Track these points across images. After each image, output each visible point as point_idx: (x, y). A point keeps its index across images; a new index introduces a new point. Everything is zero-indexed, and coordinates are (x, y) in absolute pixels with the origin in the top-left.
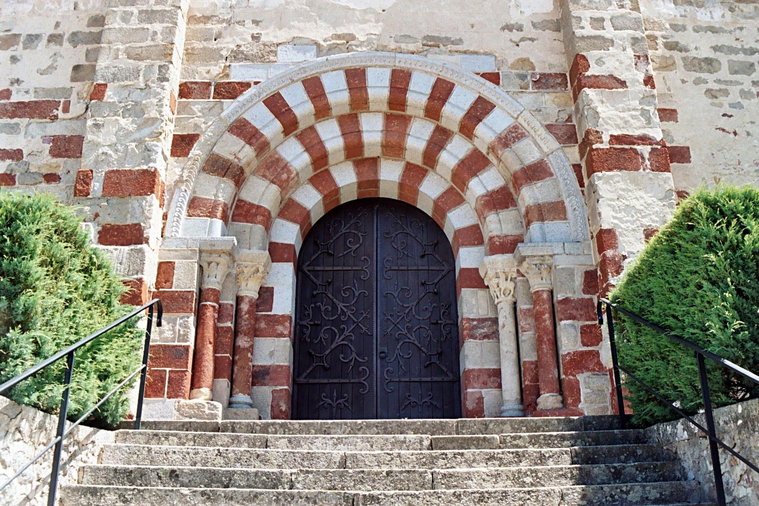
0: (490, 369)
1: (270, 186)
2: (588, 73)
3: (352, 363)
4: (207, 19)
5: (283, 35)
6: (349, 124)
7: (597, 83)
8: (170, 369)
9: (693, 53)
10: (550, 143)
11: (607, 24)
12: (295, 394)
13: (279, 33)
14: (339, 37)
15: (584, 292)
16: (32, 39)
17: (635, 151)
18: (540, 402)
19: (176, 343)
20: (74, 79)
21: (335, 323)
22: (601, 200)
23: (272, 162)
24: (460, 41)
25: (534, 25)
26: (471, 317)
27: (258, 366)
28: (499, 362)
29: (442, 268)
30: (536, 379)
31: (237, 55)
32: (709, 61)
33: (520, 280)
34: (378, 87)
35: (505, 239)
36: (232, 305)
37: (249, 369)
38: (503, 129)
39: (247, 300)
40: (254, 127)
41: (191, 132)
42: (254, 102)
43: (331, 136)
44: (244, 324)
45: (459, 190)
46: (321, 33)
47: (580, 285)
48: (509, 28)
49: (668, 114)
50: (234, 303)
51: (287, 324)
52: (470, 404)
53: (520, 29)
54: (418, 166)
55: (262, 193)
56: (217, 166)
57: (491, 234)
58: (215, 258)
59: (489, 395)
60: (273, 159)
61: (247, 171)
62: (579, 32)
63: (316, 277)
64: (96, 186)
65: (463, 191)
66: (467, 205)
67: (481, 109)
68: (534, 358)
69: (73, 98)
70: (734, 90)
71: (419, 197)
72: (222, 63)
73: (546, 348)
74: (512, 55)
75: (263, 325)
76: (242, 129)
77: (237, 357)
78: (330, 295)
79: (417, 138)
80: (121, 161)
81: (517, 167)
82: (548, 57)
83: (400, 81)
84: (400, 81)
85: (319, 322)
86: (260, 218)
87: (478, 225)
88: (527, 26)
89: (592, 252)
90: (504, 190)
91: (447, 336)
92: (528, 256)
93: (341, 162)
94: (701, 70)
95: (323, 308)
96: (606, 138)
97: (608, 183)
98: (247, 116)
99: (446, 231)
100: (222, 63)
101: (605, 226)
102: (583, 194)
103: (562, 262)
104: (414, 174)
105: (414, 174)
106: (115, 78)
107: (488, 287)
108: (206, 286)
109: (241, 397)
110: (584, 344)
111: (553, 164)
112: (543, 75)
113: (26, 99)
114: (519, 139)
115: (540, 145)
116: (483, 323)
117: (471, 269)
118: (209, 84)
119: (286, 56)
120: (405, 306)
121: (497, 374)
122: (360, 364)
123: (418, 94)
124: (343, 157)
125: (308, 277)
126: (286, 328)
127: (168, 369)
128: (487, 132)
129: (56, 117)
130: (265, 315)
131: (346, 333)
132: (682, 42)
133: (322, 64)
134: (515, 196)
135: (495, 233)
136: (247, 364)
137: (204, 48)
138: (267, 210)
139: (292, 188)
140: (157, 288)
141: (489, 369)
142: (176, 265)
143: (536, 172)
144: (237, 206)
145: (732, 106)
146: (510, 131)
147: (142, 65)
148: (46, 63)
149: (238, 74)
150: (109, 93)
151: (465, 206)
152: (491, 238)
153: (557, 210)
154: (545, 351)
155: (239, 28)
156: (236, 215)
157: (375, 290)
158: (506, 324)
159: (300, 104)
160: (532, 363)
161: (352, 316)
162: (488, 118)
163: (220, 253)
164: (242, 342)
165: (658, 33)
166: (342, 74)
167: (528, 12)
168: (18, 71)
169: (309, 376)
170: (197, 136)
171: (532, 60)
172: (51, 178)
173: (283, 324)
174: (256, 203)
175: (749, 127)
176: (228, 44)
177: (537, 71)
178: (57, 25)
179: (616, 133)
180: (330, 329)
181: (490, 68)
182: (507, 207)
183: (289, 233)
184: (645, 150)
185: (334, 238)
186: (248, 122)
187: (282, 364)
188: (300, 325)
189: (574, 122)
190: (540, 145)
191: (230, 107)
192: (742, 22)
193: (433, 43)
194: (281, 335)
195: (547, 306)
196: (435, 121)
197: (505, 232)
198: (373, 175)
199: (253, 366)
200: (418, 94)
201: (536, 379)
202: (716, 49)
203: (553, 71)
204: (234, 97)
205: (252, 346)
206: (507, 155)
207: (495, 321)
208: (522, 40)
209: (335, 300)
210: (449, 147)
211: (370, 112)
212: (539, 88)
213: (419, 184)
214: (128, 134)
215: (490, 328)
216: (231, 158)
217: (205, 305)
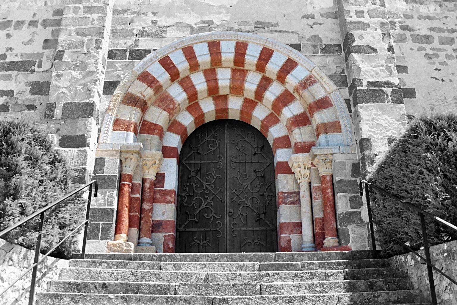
0: (295, 223)
2: (354, 44)
3: (212, 219)
4: (124, 11)
5: (170, 21)
6: (210, 75)
7: (360, 50)
8: (103, 222)
9: (418, 32)
10: (331, 86)
11: (366, 14)
13: (168, 20)
14: (204, 22)
16: (19, 24)
17: (382, 91)
19: (106, 207)
20: (44, 48)
22: (362, 121)
23: (164, 98)
24: (277, 25)
25: (322, 15)
26: (284, 191)
27: (155, 221)
28: (300, 218)
29: (266, 161)
30: (323, 228)
31: (143, 33)
32: (427, 37)
33: (313, 169)
34: (228, 53)
36: (140, 184)
37: (150, 222)
38: (303, 78)
39: (148, 181)
40: (153, 77)
42: (153, 62)
43: (199, 82)
44: (147, 195)
45: (276, 115)
46: (194, 20)
48: (306, 17)
49: (402, 69)
50: (141, 183)
52: (283, 244)
53: (313, 17)
55: (158, 116)
56: (131, 100)
57: (295, 141)
58: (129, 155)
59: (294, 238)
60: (165, 96)
61: (149, 103)
62: (348, 19)
63: (191, 167)
64: (58, 112)
65: (279, 115)
67: (289, 66)
68: (321, 216)
69: (44, 59)
70: (442, 54)
72: (134, 38)
74: (308, 33)
75: (158, 196)
76: (146, 78)
77: (143, 215)
79: (251, 83)
80: (73, 97)
81: (311, 101)
82: (329, 34)
83: (241, 49)
84: (241, 49)
86: (156, 131)
87: (288, 135)
88: (318, 16)
91: (269, 202)
92: (318, 155)
94: (422, 42)
95: (194, 186)
96: (365, 83)
97: (367, 111)
98: (149, 70)
99: (268, 139)
100: (134, 38)
101: (364, 136)
102: (351, 117)
103: (339, 158)
104: (249, 105)
105: (249, 105)
106: (69, 47)
107: (294, 173)
108: (124, 173)
109: (145, 240)
110: (352, 208)
111: (333, 99)
112: (327, 46)
113: (16, 60)
114: (312, 84)
115: (325, 88)
116: (291, 195)
118: (126, 51)
119: (173, 34)
121: (299, 225)
123: (252, 57)
124: (206, 95)
125: (186, 167)
126: (172, 198)
127: (101, 223)
128: (293, 79)
129: (34, 71)
130: (160, 190)
131: (208, 201)
132: (411, 26)
133: (194, 39)
135: (298, 141)
136: (149, 220)
137: (123, 29)
138: (161, 126)
139: (176, 113)
140: (95, 174)
143: (323, 104)
144: (143, 124)
145: (441, 64)
146: (307, 79)
147: (86, 39)
148: (28, 38)
149: (144, 44)
150: (65, 56)
152: (296, 144)
154: (328, 211)
155: (144, 17)
156: (142, 130)
158: (305, 195)
159: (181, 63)
160: (320, 219)
161: (212, 191)
162: (294, 71)
163: (132, 153)
164: (146, 206)
165: (396, 20)
166: (206, 44)
167: (318, 7)
168: (11, 43)
170: (119, 82)
171: (320, 36)
172: (31, 107)
174: (154, 122)
175: (451, 77)
176: (137, 27)
177: (324, 43)
178: (35, 15)
179: (371, 80)
181: (295, 41)
182: (305, 125)
183: (174, 141)
184: (388, 90)
185: (201, 144)
186: (149, 74)
187: (170, 219)
189: (346, 74)
190: (325, 88)
191: (138, 65)
192: (447, 13)
193: (261, 26)
194: (169, 202)
196: (262, 73)
197: (304, 140)
200: (252, 57)
201: (323, 228)
202: (431, 29)
203: (333, 43)
204: (141, 59)
205: (152, 209)
206: (305, 93)
207: (298, 193)
208: (315, 24)
209: (202, 181)
210: (270, 89)
211: (223, 68)
212: (324, 53)
213: (252, 111)
214: (77, 81)
215: (295, 198)
216: (139, 95)
217: (124, 184)
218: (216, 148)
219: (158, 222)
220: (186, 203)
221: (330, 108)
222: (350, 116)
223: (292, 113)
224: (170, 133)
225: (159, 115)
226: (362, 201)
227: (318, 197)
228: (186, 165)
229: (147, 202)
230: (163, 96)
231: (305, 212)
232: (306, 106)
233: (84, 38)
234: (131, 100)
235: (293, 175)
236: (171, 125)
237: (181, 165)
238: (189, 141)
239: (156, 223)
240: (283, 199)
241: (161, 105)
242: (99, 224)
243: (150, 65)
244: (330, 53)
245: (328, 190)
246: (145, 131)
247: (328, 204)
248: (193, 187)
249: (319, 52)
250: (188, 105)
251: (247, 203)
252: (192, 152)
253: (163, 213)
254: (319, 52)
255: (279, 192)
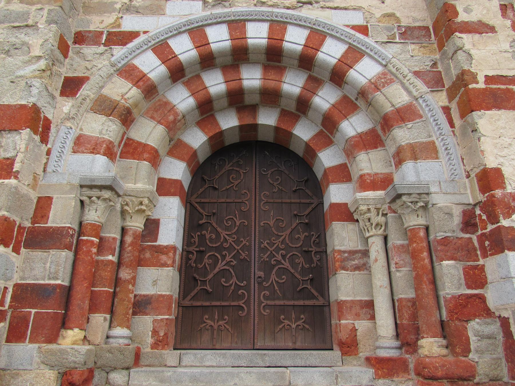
0: (362, 300)
1: (158, 126)
3: (233, 287)
7: (468, 28)
8: (36, 310)
12: (180, 317)
15: (462, 230)
18: (422, 347)
19: (47, 282)
21: (219, 249)
22: (482, 139)
23: (160, 105)
26: (343, 248)
27: (141, 295)
28: (371, 293)
29: (312, 201)
30: (414, 317)
33: (391, 216)
35: (375, 177)
36: (114, 239)
37: (129, 301)
38: (372, 76)
39: (131, 233)
40: (142, 72)
41: (81, 75)
42: (142, 49)
44: (127, 257)
45: (328, 134)
47: (458, 225)
50: (118, 237)
51: (171, 254)
54: (292, 113)
55: (150, 132)
56: (105, 107)
57: (361, 173)
59: (362, 326)
60: (162, 103)
61: (135, 111)
63: (203, 208)
65: (332, 133)
66: (335, 146)
68: (411, 294)
71: (292, 140)
73: (427, 288)
75: (148, 255)
76: (130, 72)
77: (118, 289)
78: (214, 224)
85: (204, 249)
86: (146, 155)
87: (346, 164)
89: (469, 191)
90: (372, 132)
92: (404, 194)
93: (225, 109)
95: (208, 236)
96: (481, 79)
99: (315, 169)
102: (454, 135)
107: (357, 221)
110: (469, 287)
111: (422, 106)
112: (408, 28)
114: (388, 85)
116: (353, 255)
117: (341, 204)
118: (102, 33)
120: (279, 234)
121: (370, 305)
122: (240, 287)
124: (226, 104)
125: (195, 208)
127: (33, 311)
130: (150, 245)
131: (228, 259)
134: (383, 138)
135: (366, 171)
136: (127, 296)
138: (154, 148)
139: (179, 129)
140: (33, 223)
141: (361, 301)
142: (54, 200)
143: (406, 114)
144: (125, 144)
146: (379, 77)
149: (129, 23)
151: (333, 147)
152: (361, 176)
153: (427, 151)
154: (426, 291)
156: (124, 153)
157: (253, 220)
158: (378, 259)
160: (409, 300)
161: (233, 243)
162: (358, 66)
164: (125, 274)
169: (193, 298)
170: (88, 78)
171: (398, 15)
173: (166, 254)
174: (143, 141)
179: (491, 73)
180: (214, 255)
182: (376, 148)
185: (219, 174)
186: (136, 67)
187: (164, 293)
188: (187, 251)
189: (440, 69)
194: (164, 265)
195: (425, 244)
196: (307, 71)
197: (376, 170)
198: (252, 120)
199: (135, 296)
201: (414, 317)
203: (417, 24)
204: (124, 44)
205: (134, 278)
209: (218, 229)
211: (250, 63)
212: (406, 39)
213: (292, 128)
216: (118, 98)
217: (82, 240)
218: (240, 181)
219: (145, 298)
220: (195, 262)
221: (418, 120)
222: (452, 133)
223: (355, 129)
224: (170, 159)
225: (152, 131)
226: (485, 275)
227: (402, 262)
228: (196, 205)
229: (127, 267)
230: (159, 103)
231: (380, 287)
232: (379, 119)
233: (30, 7)
234: (105, 107)
235: (357, 223)
236: (173, 147)
237: (188, 204)
238: (203, 171)
239: (142, 300)
240: (341, 262)
241: (155, 116)
242: (30, 312)
243: (138, 54)
244: (413, 39)
245: (422, 253)
246: (129, 155)
247: (425, 279)
248: (206, 239)
249: (397, 37)
250: (199, 119)
251: (285, 264)
252: (206, 186)
253: (155, 283)
254: (397, 37)
255: (334, 251)
